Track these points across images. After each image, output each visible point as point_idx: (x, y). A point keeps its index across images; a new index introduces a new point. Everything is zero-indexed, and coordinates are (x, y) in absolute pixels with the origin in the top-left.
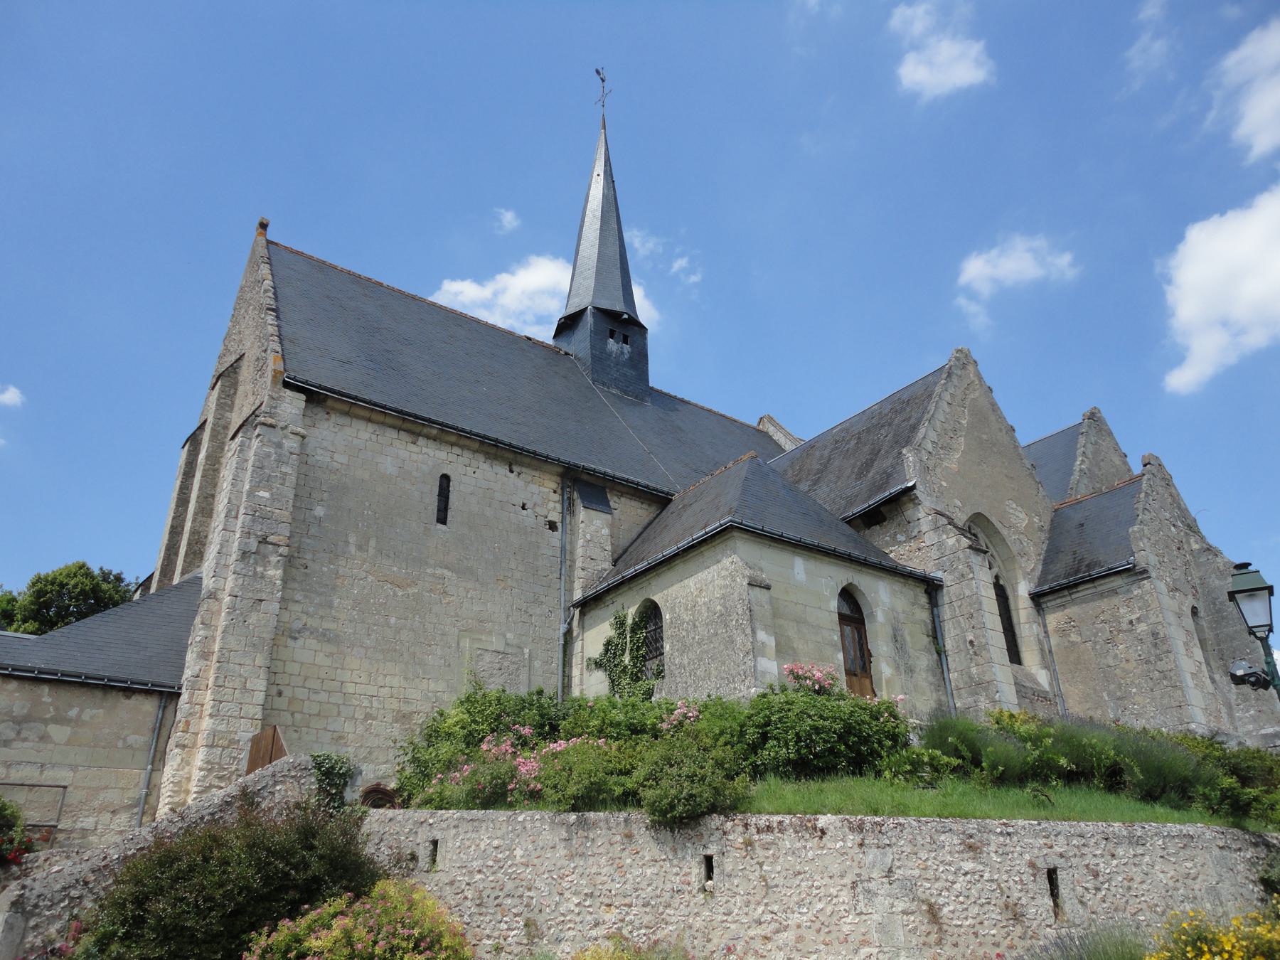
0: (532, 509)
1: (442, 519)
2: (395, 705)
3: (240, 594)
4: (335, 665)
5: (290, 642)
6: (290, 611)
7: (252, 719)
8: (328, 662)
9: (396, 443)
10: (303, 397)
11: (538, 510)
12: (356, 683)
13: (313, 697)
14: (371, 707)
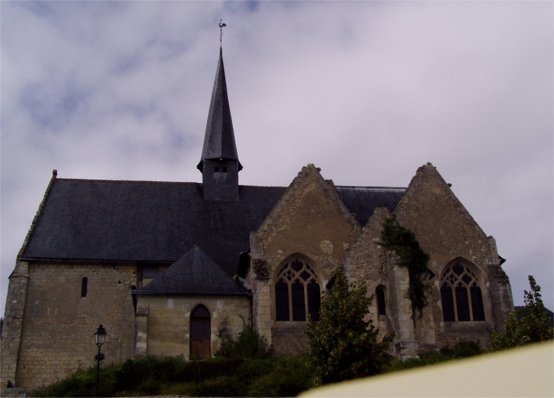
0: (123, 283)
1: (84, 294)
2: (65, 367)
3: (7, 337)
4: (43, 356)
5: (28, 350)
6: (27, 339)
7: (12, 377)
8: (41, 355)
9: (65, 270)
10: (27, 263)
11: (126, 282)
12: (51, 361)
13: (36, 367)
14: (57, 368)
